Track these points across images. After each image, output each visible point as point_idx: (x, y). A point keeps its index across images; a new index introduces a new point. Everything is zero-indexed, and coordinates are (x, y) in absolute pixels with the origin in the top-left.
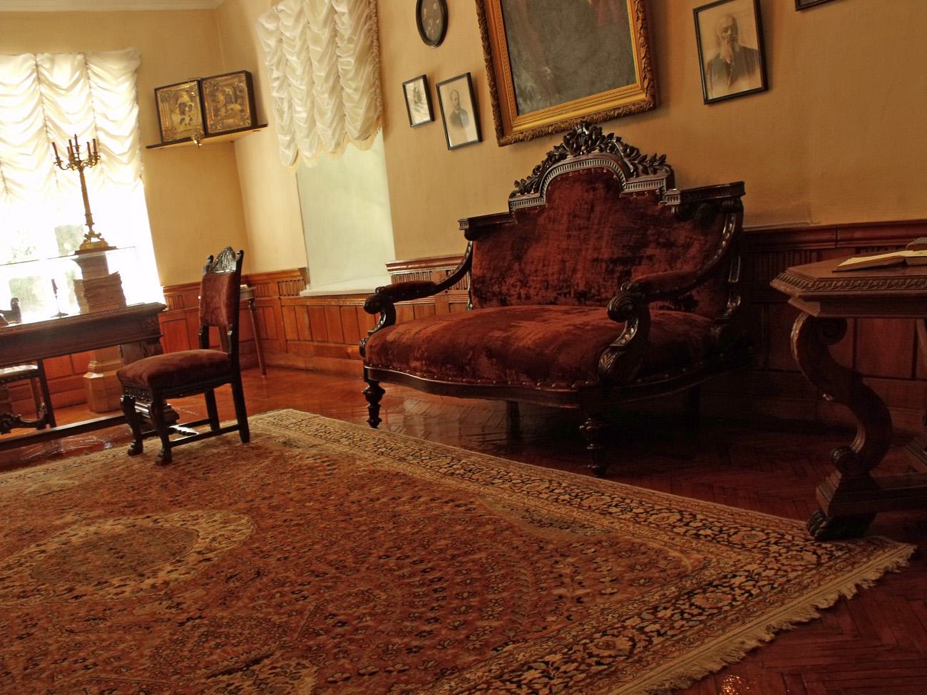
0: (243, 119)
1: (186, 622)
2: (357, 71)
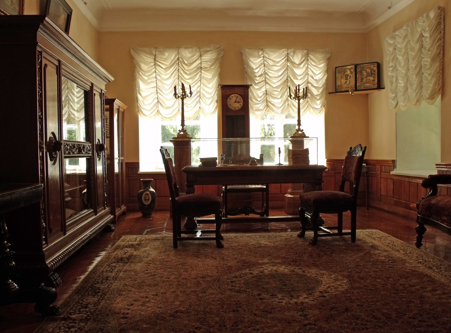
0: (374, 84)
1: (307, 325)
2: (431, 65)
